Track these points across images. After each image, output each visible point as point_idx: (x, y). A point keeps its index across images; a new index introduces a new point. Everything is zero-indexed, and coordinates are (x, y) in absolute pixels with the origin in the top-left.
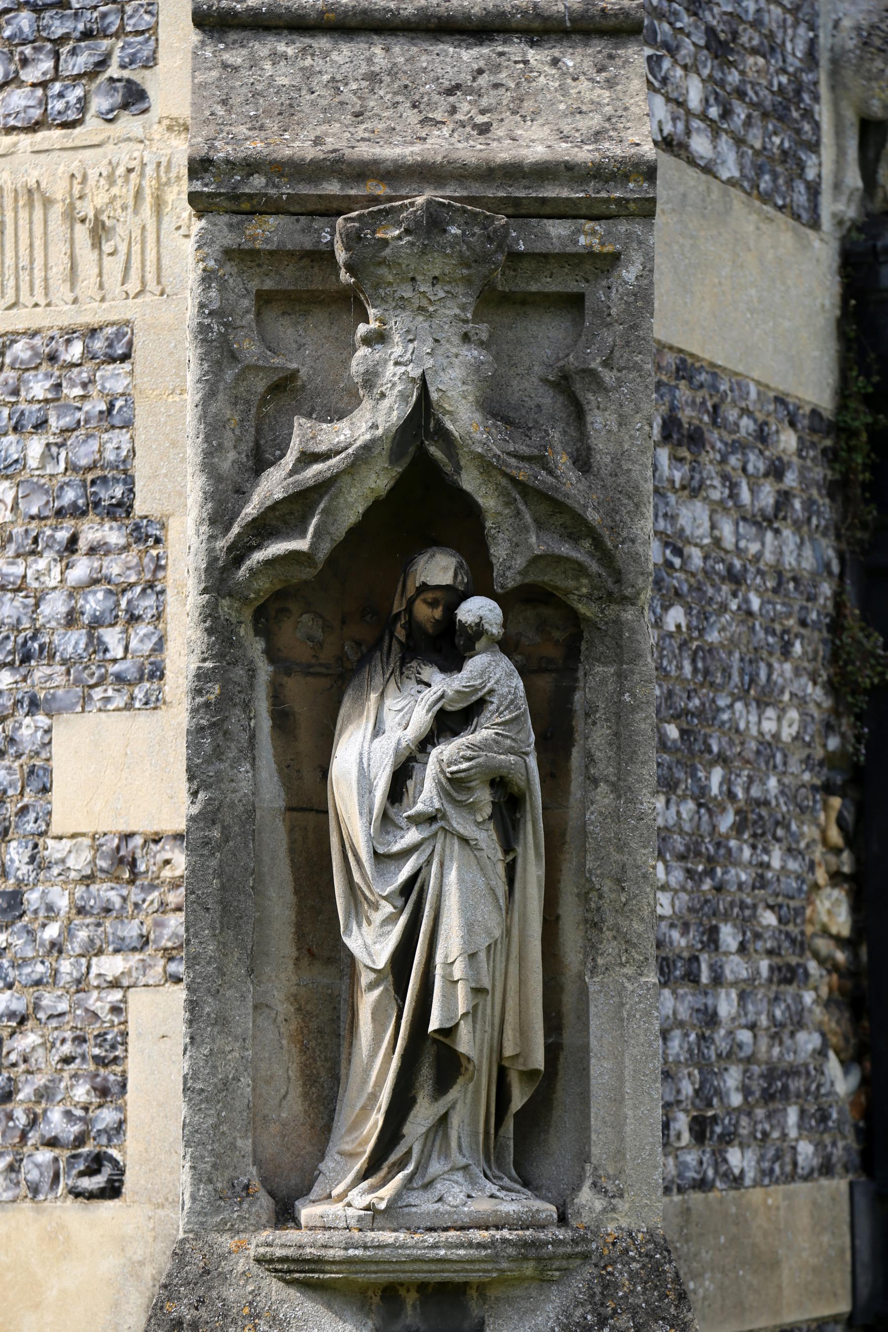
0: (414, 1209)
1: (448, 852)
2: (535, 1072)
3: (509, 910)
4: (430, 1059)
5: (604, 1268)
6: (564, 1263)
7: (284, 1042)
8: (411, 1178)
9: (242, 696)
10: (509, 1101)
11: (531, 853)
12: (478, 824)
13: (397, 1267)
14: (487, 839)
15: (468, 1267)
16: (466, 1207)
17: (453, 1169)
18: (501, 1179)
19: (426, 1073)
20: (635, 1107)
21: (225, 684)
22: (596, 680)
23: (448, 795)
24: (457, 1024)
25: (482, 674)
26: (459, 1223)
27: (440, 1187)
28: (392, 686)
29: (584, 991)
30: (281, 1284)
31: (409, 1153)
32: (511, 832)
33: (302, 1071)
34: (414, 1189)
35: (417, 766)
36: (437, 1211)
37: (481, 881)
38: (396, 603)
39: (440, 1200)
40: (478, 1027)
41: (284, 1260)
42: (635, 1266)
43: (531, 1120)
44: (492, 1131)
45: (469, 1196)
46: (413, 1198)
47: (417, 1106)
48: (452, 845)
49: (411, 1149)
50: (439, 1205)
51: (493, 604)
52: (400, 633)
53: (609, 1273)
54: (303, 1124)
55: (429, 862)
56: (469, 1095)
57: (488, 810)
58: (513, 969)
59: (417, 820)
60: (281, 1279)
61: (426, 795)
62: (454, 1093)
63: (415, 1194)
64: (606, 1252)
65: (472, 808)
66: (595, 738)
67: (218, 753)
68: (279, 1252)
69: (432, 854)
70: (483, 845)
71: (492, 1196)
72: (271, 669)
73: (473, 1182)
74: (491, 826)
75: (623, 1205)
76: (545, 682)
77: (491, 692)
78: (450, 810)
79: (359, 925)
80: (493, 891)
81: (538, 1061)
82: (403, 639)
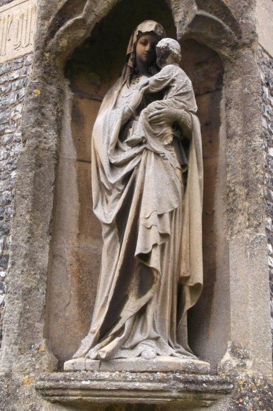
0: (124, 360)
1: (148, 160)
2: (198, 284)
3: (183, 198)
4: (136, 270)
5: (238, 400)
6: (213, 396)
7: (69, 276)
8: (124, 342)
9: (53, 99)
10: (184, 304)
11: (195, 165)
12: (166, 146)
13: (111, 393)
14: (171, 155)
15: (153, 394)
16: (153, 357)
17: (149, 338)
18: (179, 348)
19: (134, 282)
20: (255, 306)
21: (43, 90)
22: (234, 88)
23: (149, 131)
24: (151, 252)
25: (169, 71)
26: (150, 369)
27: (140, 348)
28: (125, 86)
29: (227, 243)
30: (49, 403)
31: (122, 328)
32: (185, 159)
33: (78, 291)
34: (125, 349)
35: (135, 121)
36: (137, 362)
37: (166, 177)
38: (128, 49)
39: (140, 355)
40: (165, 258)
41: (50, 388)
42: (256, 399)
43: (195, 318)
44: (175, 321)
45: (158, 355)
46: (123, 353)
47: (129, 301)
48: (150, 156)
49: (101, 299)
50: (139, 358)
51: (177, 43)
52: (130, 63)
53: (240, 403)
54: (78, 320)
55: (138, 166)
56: (160, 298)
57: (171, 139)
58: (186, 229)
59: (134, 144)
60: (49, 400)
61: (138, 131)
62: (149, 294)
63: (126, 351)
64: (239, 390)
65: (162, 137)
66: (231, 116)
67: (39, 123)
68: (47, 384)
69: (140, 162)
70: (167, 156)
71: (172, 355)
72: (72, 94)
73: (161, 346)
74: (173, 149)
75: (249, 363)
76: (206, 98)
77: (173, 81)
78: (149, 138)
79: (102, 204)
80: (173, 182)
81: (198, 277)
82: (132, 66)
